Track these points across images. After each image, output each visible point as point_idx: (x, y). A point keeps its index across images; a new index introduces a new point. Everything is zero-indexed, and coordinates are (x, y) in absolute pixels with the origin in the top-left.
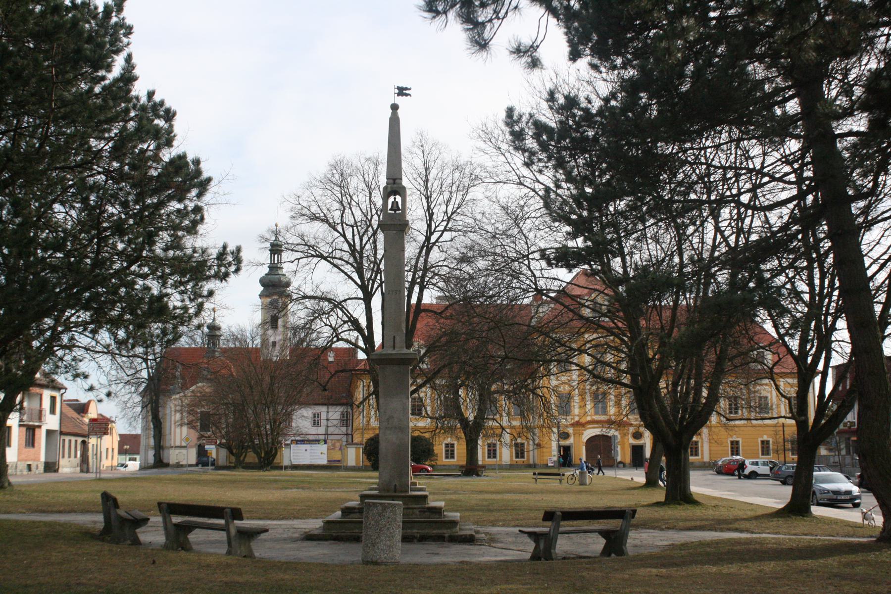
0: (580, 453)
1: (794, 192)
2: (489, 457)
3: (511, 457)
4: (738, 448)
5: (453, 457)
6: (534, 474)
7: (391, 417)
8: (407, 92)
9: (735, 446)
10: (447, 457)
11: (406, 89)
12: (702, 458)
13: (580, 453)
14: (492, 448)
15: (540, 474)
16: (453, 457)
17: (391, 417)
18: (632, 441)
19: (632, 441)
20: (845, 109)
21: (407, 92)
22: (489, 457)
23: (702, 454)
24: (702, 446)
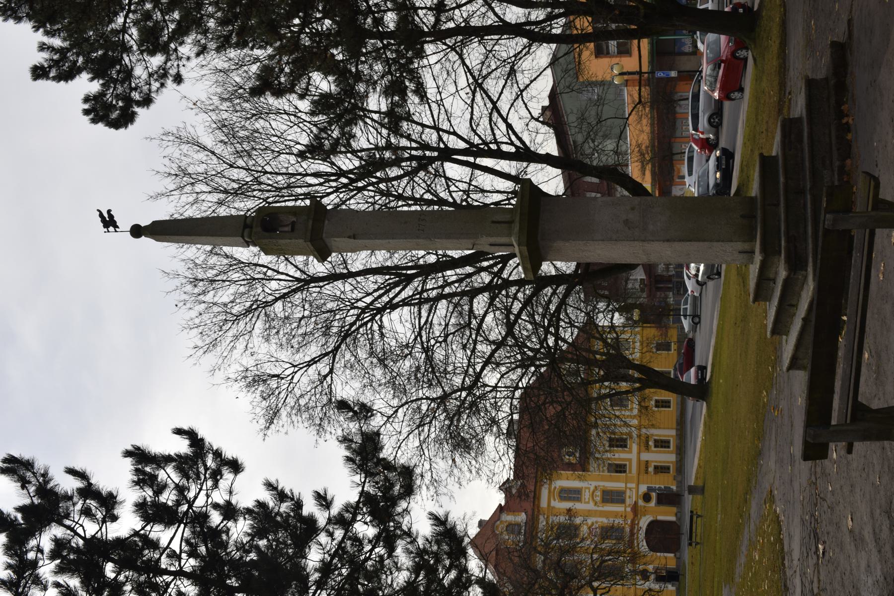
0: (668, 560)
1: (448, 165)
2: (669, 447)
3: (668, 452)
4: (663, 401)
5: (669, 402)
6: (690, 544)
7: (626, 222)
8: (106, 215)
9: (659, 444)
10: (669, 407)
11: (101, 215)
12: (672, 436)
13: (668, 560)
14: (660, 404)
15: (691, 538)
16: (669, 402)
17: (626, 222)
18: (653, 503)
19: (653, 503)
20: (250, 515)
21: (106, 215)
22: (669, 447)
23: (669, 436)
24: (660, 436)
